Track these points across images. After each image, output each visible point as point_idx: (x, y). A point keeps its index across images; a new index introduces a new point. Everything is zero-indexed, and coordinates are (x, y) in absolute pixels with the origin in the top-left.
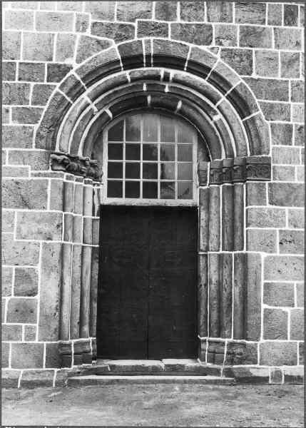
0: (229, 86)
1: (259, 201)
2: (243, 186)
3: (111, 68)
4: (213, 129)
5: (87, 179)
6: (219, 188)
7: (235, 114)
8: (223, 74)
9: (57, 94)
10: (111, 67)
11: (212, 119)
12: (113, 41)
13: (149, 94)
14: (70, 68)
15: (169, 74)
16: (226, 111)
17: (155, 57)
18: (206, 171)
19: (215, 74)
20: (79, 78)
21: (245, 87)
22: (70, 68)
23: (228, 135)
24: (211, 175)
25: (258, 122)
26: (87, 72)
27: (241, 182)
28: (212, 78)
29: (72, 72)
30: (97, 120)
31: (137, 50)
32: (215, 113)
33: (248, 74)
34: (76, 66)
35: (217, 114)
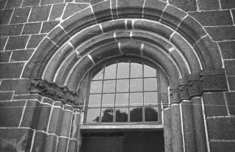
0: (177, 20)
1: (229, 78)
2: (200, 100)
3: (88, 21)
4: (170, 60)
5: (66, 105)
6: (179, 106)
7: (185, 42)
8: (172, 13)
9: (46, 39)
10: (87, 21)
11: (168, 52)
12: (90, 4)
13: (119, 42)
14: (58, 22)
15: (131, 21)
16: (178, 42)
17: (120, 9)
18: (167, 94)
19: (166, 14)
20: (62, 28)
21: (192, 19)
22: (58, 22)
23: (182, 61)
24: (171, 95)
25: (207, 43)
26: (69, 24)
27: (198, 96)
28: (163, 18)
29: (59, 25)
30: (81, 61)
31: (105, 7)
32: (170, 46)
33: (193, 10)
34: (62, 21)
35: (172, 47)
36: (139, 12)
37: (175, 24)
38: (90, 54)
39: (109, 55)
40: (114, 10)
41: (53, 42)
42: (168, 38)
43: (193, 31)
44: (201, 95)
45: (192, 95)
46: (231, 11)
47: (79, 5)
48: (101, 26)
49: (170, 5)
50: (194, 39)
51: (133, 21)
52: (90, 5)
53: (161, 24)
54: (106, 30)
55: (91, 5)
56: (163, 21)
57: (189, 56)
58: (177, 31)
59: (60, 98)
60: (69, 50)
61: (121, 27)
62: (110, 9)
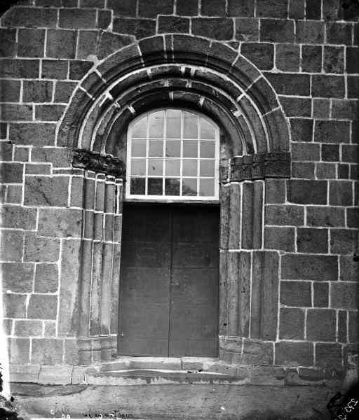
12: (134, 37)
14: (91, 64)
17: (176, 52)
26: (108, 69)
34: (98, 63)
36: (203, 60)
37: (245, 84)
38: (133, 106)
39: (153, 100)
40: (169, 52)
41: (88, 94)
42: (235, 99)
43: (265, 98)
44: (264, 179)
45: (255, 177)
46: (348, 313)
47: (120, 38)
48: (149, 70)
49: (234, 37)
50: (266, 109)
51: (193, 69)
52: (135, 40)
53: (208, 39)
54: (156, 76)
55: (137, 39)
56: (230, 76)
57: (257, 130)
58: (247, 93)
59: (104, 169)
60: (108, 103)
61: (174, 74)
62: (163, 51)
